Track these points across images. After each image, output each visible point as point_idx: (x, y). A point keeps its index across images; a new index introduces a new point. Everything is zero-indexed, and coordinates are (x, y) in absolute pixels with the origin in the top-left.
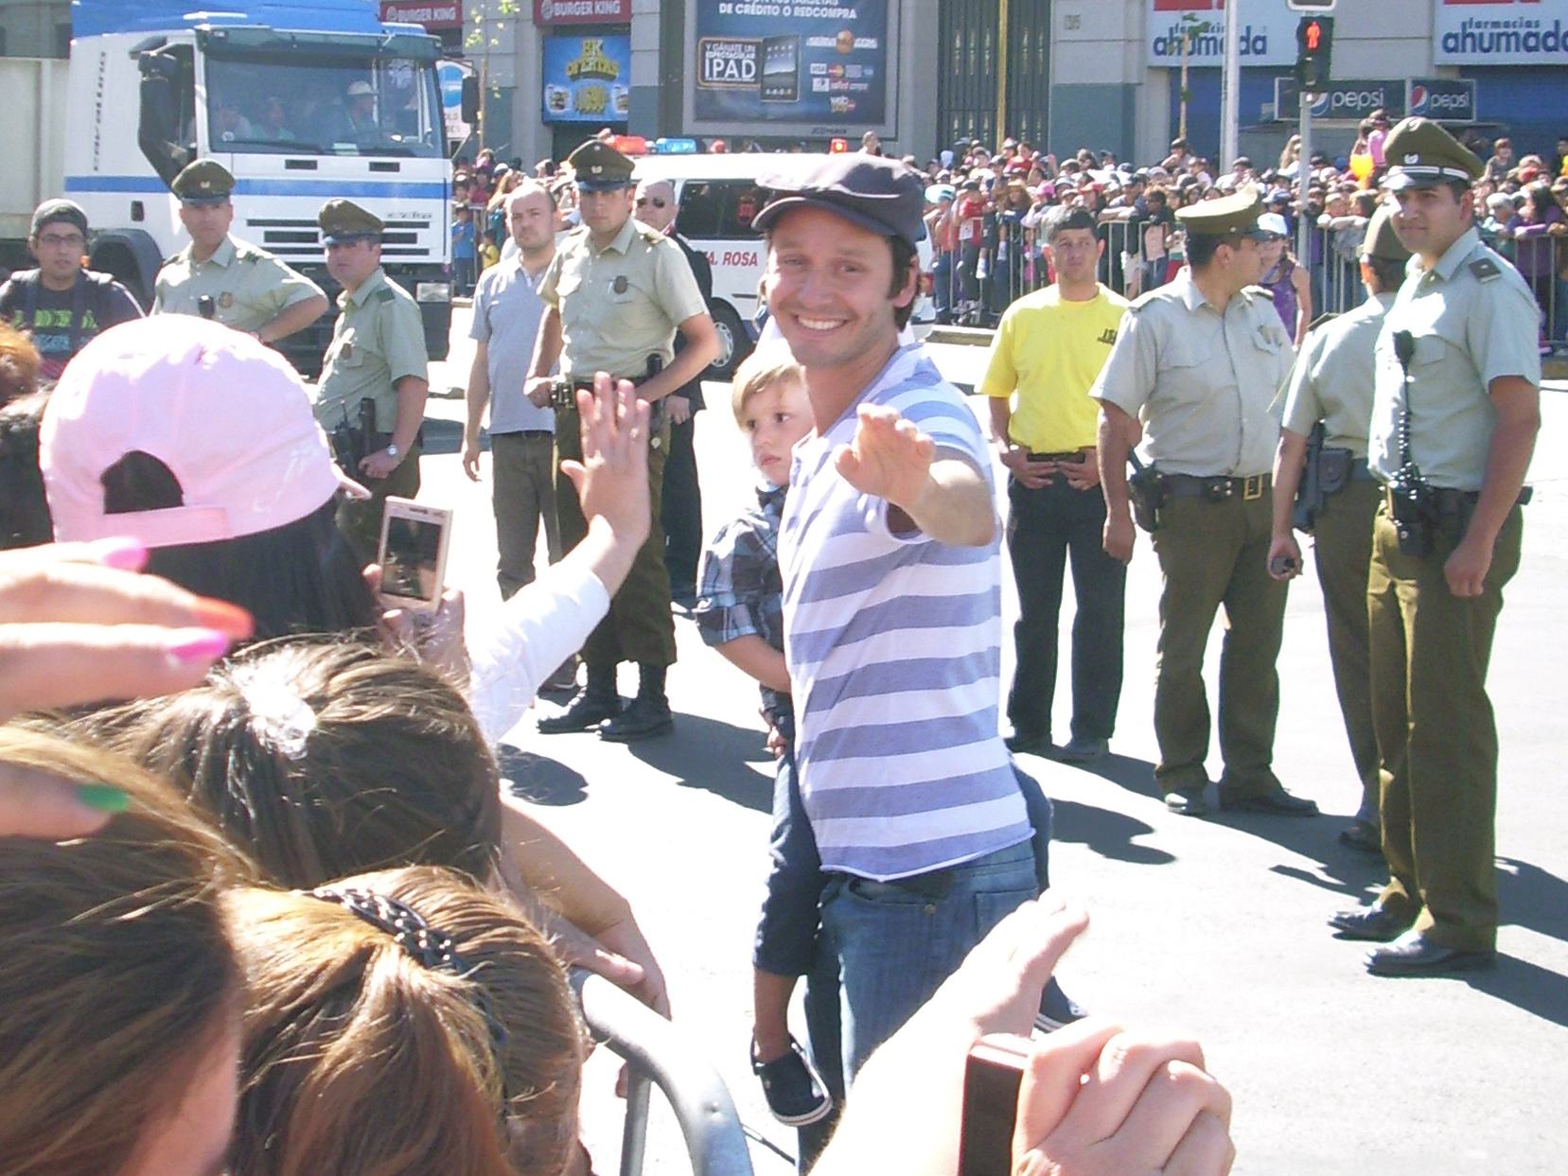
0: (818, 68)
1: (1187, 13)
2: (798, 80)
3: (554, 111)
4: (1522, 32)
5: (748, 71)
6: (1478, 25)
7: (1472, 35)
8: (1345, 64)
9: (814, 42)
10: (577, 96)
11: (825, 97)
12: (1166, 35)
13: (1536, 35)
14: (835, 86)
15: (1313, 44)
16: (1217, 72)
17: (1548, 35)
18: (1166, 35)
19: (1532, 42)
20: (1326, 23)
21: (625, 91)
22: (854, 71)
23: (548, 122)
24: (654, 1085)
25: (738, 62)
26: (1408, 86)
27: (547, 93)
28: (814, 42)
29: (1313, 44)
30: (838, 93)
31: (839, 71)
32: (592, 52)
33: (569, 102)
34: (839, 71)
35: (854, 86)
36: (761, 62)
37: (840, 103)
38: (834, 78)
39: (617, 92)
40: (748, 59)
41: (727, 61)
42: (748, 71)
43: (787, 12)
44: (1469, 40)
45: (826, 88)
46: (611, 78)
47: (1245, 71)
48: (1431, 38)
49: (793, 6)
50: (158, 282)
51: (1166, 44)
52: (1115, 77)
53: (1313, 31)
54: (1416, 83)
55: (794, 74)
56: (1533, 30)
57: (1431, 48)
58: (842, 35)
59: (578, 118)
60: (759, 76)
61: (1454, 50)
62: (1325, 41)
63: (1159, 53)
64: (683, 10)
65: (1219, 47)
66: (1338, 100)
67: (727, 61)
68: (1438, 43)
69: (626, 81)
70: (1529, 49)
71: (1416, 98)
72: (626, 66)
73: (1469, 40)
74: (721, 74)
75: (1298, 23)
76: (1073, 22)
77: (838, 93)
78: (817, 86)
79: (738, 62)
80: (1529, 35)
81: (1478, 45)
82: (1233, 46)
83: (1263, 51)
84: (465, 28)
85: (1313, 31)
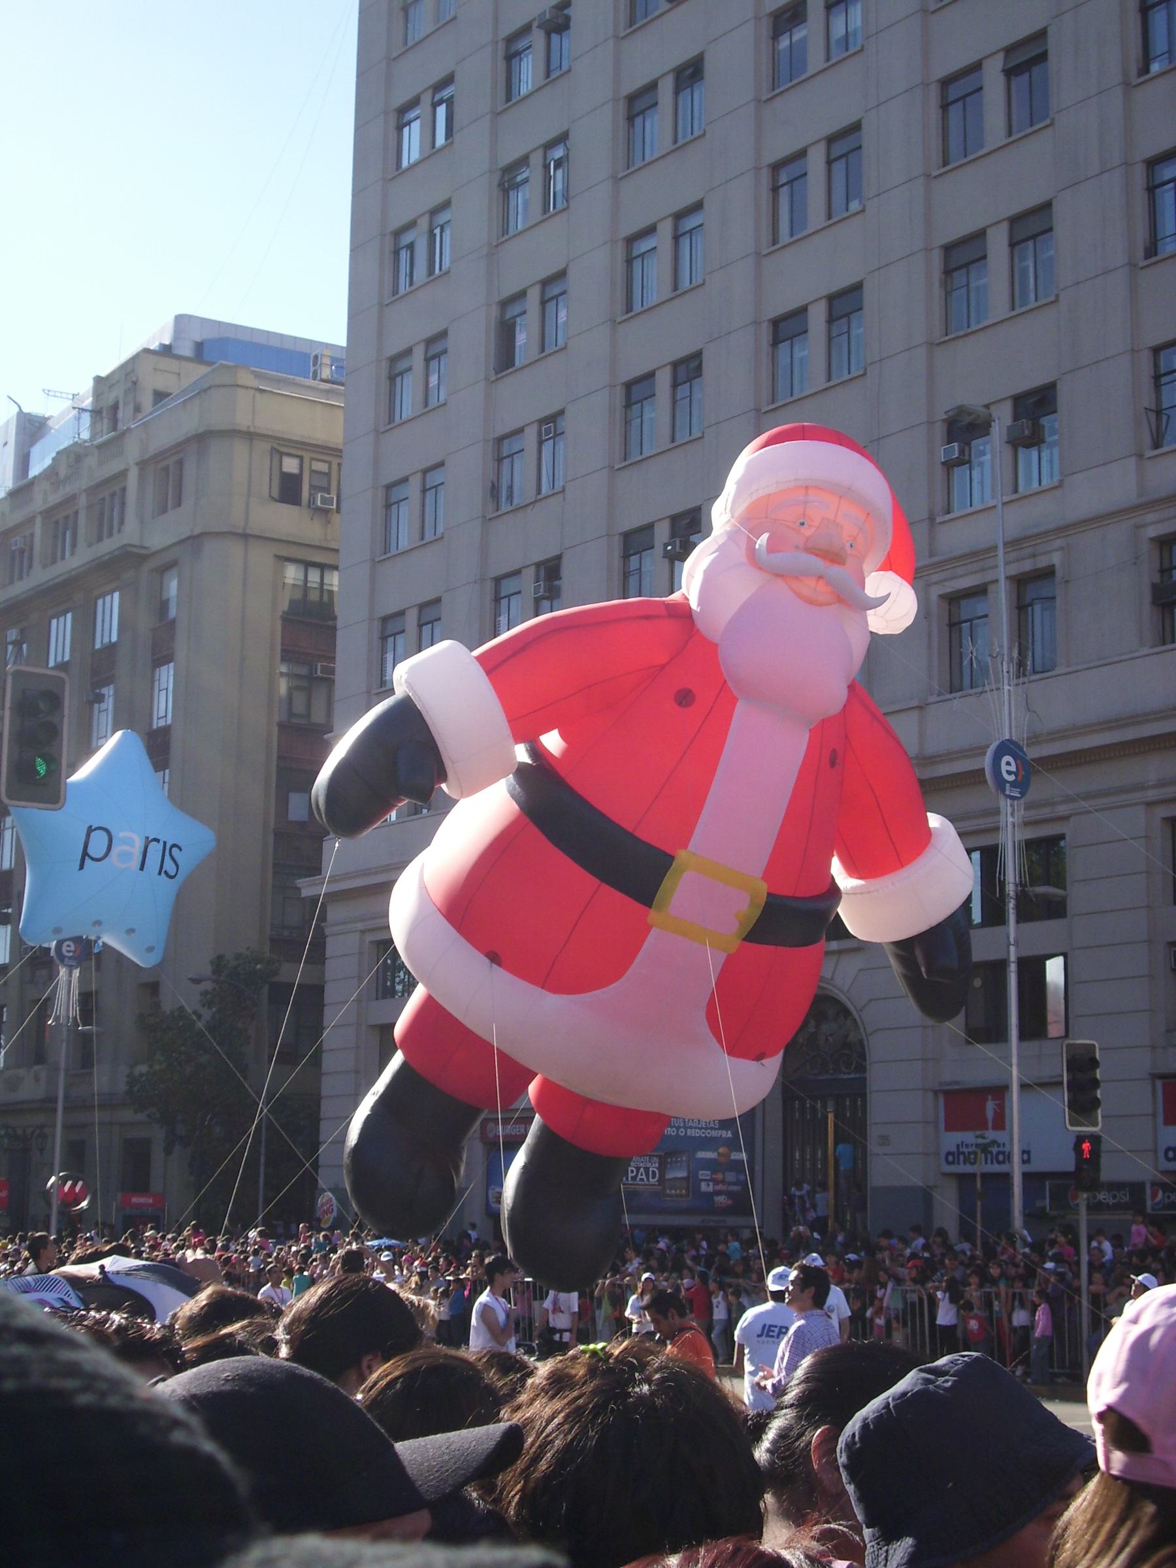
0: (704, 1174)
1: (978, 1133)
2: (691, 1181)
5: (654, 1177)
7: (963, 1153)
8: (1109, 1171)
9: (701, 1155)
11: (710, 1196)
12: (955, 1149)
13: (1003, 1153)
14: (720, 1187)
15: (1087, 1155)
16: (1007, 1177)
18: (955, 1149)
19: (1001, 1158)
20: (1095, 1140)
22: (731, 1176)
25: (647, 1170)
26: (1148, 1186)
27: (490, 1192)
28: (701, 1155)
29: (1087, 1155)
30: (719, 1193)
31: (720, 1176)
34: (720, 1176)
35: (732, 1188)
36: (662, 1168)
37: (721, 1200)
38: (716, 1182)
40: (654, 1167)
41: (638, 1169)
42: (654, 1177)
43: (682, 1132)
44: (962, 1157)
45: (711, 1189)
47: (1026, 1176)
48: (1155, 1151)
49: (686, 1128)
51: (952, 1157)
52: (917, 1181)
53: (1086, 1146)
54: (1153, 1184)
55: (687, 1179)
56: (1001, 1149)
57: (1156, 1160)
58: (721, 1150)
60: (662, 1180)
61: (953, 1163)
62: (1096, 1153)
63: (949, 1163)
64: (1164, 1100)
65: (1008, 1157)
66: (1169, 1197)
67: (638, 1169)
68: (1161, 1154)
70: (999, 1162)
71: (1154, 1195)
73: (962, 1157)
74: (634, 1178)
75: (1074, 1140)
76: (884, 1140)
77: (719, 1193)
78: (704, 1187)
79: (647, 1170)
80: (999, 1153)
82: (1016, 1158)
85: (1086, 1146)
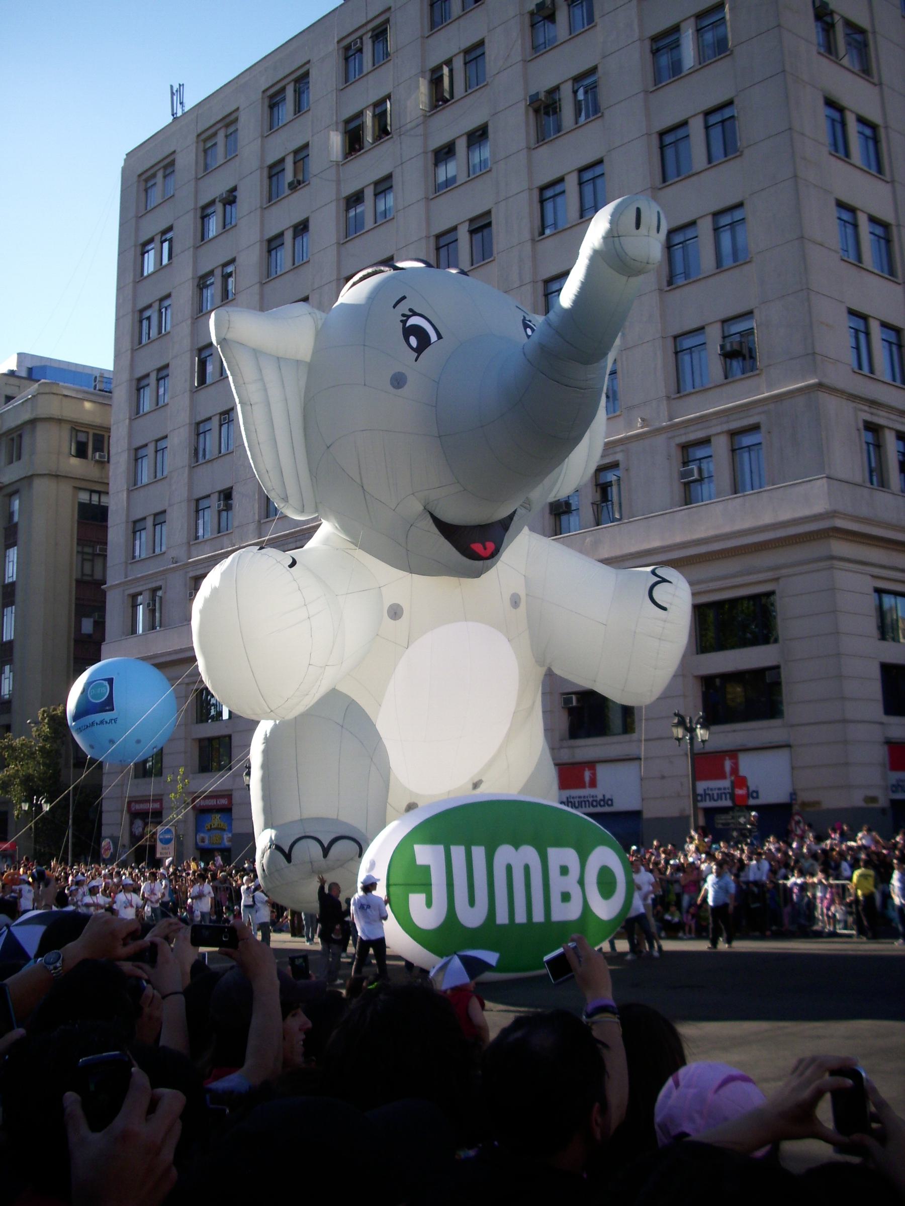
3: (201, 844)
4: (591, 799)
6: (712, 789)
10: (210, 837)
17: (601, 800)
21: (230, 835)
23: (198, 848)
24: (118, 963)
32: (216, 820)
33: (207, 841)
39: (227, 836)
46: (224, 830)
50: (658, 1119)
59: (210, 846)
69: (230, 831)
70: (593, 806)
72: (230, 825)
81: (712, 798)
83: (757, 797)
84: (164, 812)
